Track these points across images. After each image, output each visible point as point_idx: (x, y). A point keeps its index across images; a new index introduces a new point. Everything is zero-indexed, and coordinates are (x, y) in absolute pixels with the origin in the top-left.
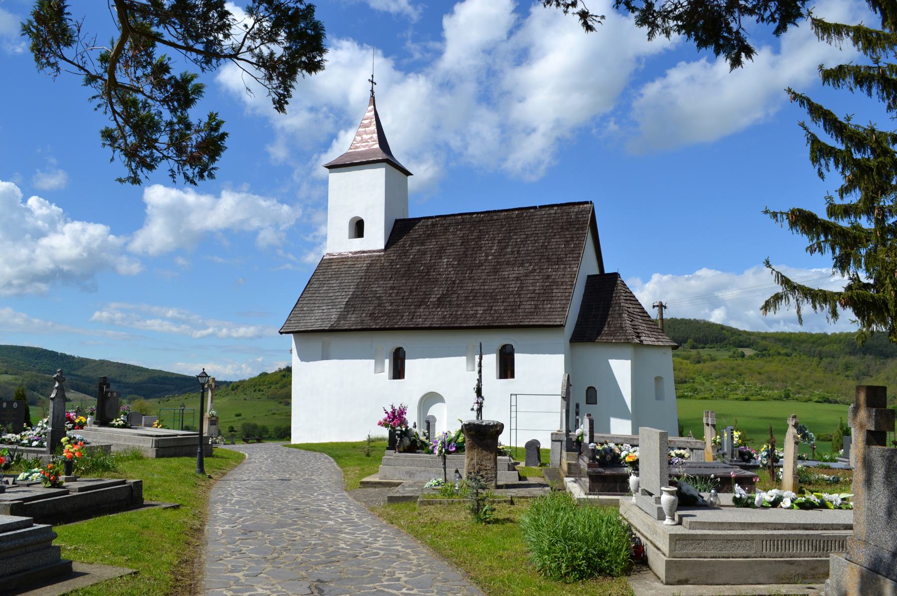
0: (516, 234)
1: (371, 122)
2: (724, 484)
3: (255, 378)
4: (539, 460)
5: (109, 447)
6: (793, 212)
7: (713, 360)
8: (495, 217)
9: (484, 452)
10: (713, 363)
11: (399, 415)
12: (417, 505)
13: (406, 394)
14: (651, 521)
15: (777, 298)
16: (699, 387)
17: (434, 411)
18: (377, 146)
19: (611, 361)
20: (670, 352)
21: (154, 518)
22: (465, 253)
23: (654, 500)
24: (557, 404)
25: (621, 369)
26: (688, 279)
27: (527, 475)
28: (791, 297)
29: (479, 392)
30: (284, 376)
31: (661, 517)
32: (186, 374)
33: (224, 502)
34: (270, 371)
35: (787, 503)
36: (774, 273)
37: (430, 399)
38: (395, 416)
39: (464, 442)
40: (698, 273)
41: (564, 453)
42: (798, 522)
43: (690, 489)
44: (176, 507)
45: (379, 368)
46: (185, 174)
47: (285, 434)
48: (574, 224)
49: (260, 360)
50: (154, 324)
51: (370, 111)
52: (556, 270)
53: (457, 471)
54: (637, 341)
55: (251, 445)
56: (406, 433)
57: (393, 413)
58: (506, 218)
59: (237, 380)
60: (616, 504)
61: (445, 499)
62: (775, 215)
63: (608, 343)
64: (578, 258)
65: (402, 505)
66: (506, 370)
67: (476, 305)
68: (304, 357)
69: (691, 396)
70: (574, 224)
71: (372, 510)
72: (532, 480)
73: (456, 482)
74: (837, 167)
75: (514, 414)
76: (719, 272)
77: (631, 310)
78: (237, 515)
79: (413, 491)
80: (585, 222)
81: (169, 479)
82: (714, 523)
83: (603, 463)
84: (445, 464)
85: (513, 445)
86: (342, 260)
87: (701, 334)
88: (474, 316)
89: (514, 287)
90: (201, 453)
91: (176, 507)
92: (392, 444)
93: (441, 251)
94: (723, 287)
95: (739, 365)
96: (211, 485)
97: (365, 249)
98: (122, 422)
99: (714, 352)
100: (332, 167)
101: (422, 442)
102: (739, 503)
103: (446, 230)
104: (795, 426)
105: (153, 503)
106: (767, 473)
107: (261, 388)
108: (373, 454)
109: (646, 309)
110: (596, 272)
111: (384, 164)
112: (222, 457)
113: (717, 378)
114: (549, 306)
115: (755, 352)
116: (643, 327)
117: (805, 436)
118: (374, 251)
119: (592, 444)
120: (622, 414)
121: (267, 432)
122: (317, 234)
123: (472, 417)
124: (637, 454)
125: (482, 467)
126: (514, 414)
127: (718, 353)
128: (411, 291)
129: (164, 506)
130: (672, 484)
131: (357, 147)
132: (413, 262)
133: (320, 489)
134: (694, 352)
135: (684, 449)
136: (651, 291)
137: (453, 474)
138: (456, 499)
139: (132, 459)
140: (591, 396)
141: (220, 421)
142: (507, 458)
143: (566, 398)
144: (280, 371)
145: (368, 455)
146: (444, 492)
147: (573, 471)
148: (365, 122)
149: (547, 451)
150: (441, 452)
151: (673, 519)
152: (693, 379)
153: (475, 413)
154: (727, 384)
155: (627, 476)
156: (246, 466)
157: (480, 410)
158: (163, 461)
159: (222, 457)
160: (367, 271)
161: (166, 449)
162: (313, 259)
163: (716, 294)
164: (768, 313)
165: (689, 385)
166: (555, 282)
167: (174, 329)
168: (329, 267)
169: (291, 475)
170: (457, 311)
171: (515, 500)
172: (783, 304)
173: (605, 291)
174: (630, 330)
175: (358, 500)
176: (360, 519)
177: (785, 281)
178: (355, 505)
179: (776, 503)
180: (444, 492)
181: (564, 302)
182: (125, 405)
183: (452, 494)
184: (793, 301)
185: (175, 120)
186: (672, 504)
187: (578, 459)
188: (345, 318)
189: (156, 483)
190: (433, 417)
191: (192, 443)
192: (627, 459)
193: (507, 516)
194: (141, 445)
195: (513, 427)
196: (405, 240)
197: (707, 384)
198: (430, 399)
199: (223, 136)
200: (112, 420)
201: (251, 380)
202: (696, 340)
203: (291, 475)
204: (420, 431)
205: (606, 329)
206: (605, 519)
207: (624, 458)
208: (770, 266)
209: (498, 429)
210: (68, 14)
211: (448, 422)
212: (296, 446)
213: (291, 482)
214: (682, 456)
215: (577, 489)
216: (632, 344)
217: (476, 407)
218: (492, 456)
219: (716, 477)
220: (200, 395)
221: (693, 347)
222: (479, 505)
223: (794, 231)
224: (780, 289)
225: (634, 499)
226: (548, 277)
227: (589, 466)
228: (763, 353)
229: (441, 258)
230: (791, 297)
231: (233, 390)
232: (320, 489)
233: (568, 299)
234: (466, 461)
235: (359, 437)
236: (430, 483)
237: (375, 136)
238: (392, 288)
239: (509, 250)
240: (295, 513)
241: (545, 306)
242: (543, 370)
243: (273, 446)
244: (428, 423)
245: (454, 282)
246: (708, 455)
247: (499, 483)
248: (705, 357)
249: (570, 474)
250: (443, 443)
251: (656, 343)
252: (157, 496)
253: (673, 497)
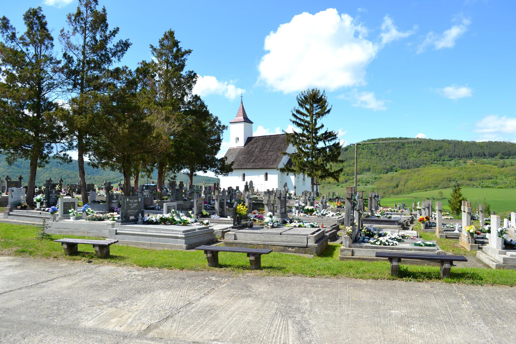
7: (512, 165)
10: (513, 167)
69: (492, 187)
74: (181, 184)
87: (507, 150)
165: (493, 180)
196: (249, 144)
197: (505, 180)
202: (503, 154)
221: (502, 158)
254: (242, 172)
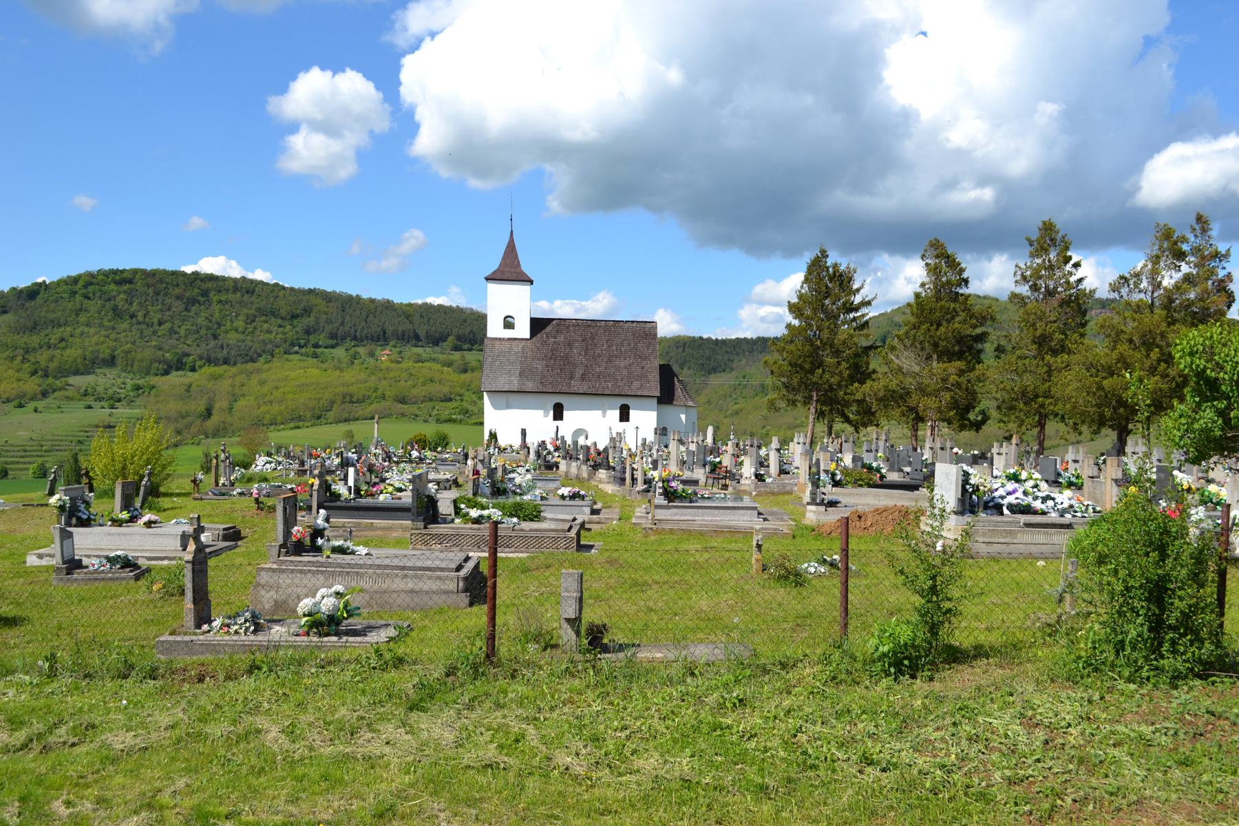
16: (470, 408)
45: (546, 415)
69: (461, 421)
87: (468, 330)
134: (457, 356)
195: (22, 453)
202: (459, 338)
221: (456, 348)
242: (645, 421)
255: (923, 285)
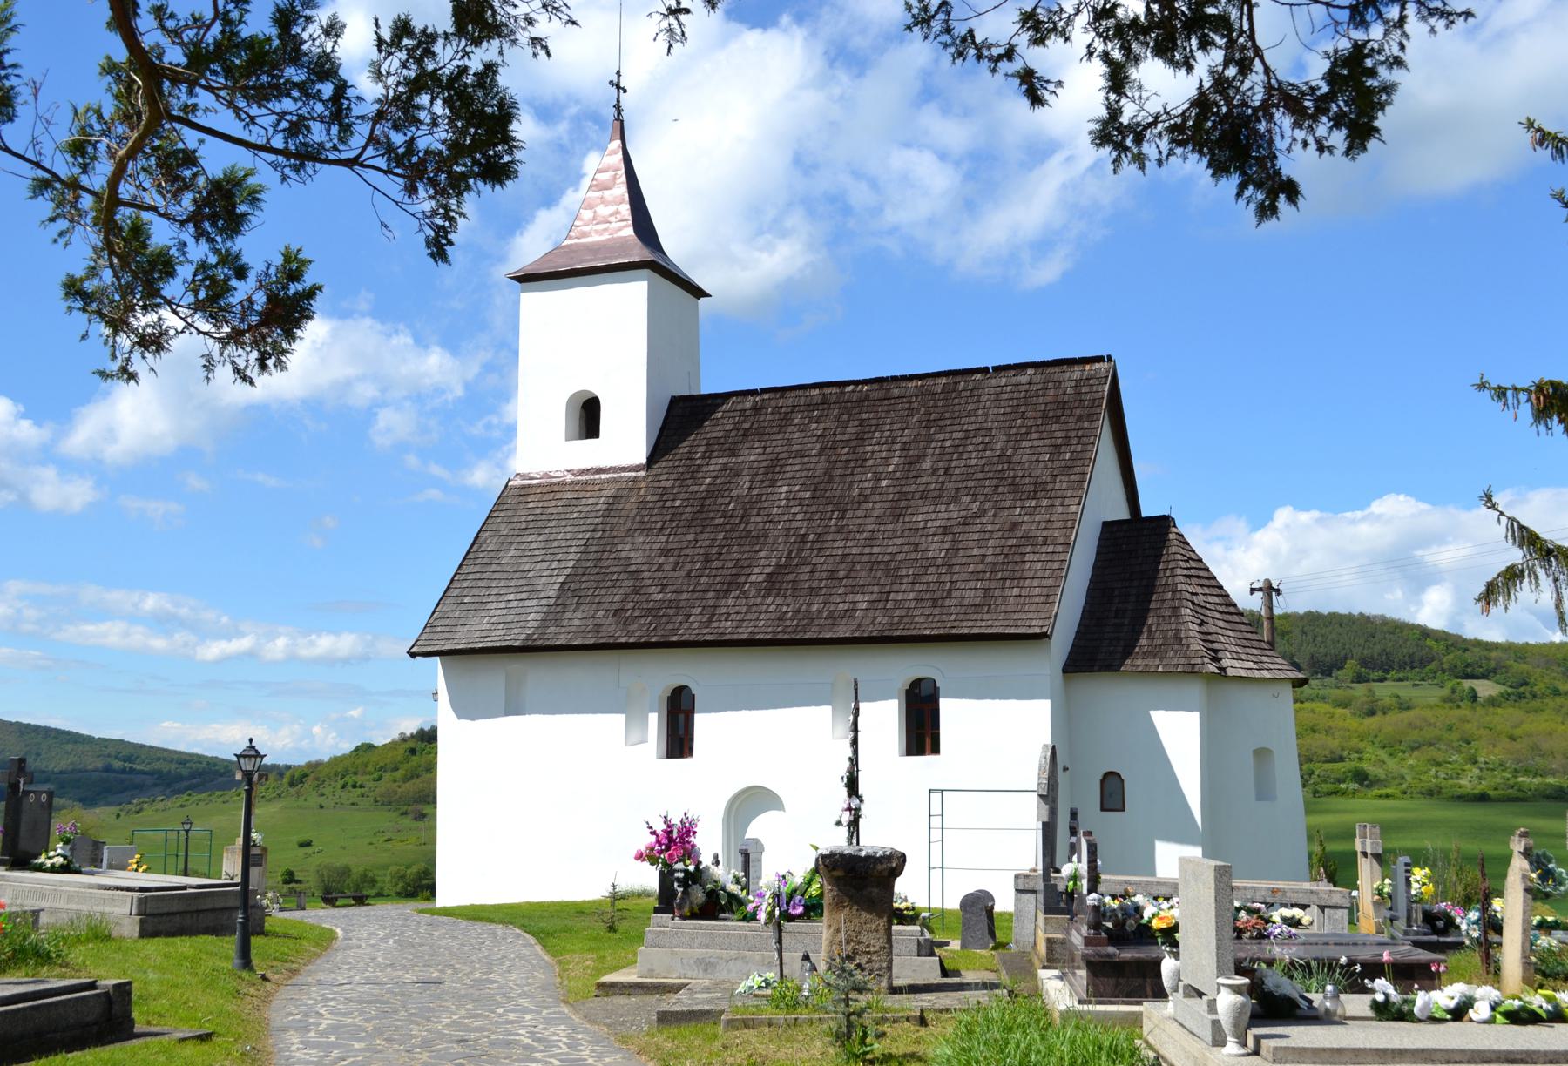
0: (941, 429)
1: (615, 178)
2: (1355, 977)
3: (344, 757)
4: (992, 934)
5: (36, 914)
6: (1540, 388)
7: (1404, 706)
8: (896, 392)
9: (865, 916)
11: (681, 838)
12: (720, 1029)
13: (695, 792)
14: (1198, 1047)
15: (1512, 576)
17: (758, 828)
18: (630, 231)
19: (1152, 713)
20: (1287, 692)
21: (162, 1058)
22: (828, 473)
23: (1205, 1007)
24: (1028, 813)
25: (1179, 732)
26: (1353, 522)
27: (961, 967)
28: (1541, 573)
29: (852, 785)
30: (413, 751)
31: (1219, 1041)
32: (179, 748)
33: (304, 1028)
34: (380, 740)
35: (1481, 1011)
36: (1504, 520)
37: (752, 801)
38: (671, 840)
39: (821, 896)
40: (1377, 507)
41: (1041, 917)
42: (1496, 1047)
43: (1276, 981)
44: (204, 1038)
45: (634, 733)
46: (233, 363)
47: (421, 885)
48: (1075, 404)
49: (355, 713)
50: (111, 633)
51: (614, 152)
52: (1033, 511)
53: (806, 957)
54: (1212, 668)
55: (344, 911)
56: (696, 877)
57: (668, 832)
58: (921, 393)
59: (301, 761)
60: (1136, 1020)
61: (780, 1016)
62: (1501, 393)
63: (1146, 673)
64: (1080, 484)
65: (687, 1030)
66: (922, 734)
67: (854, 589)
68: (465, 710)
69: (1354, 792)
70: (1075, 404)
71: (624, 1040)
72: (969, 977)
73: (803, 980)
75: (936, 835)
76: (1424, 506)
77: (1199, 599)
78: (335, 1053)
79: (711, 1001)
80: (1095, 403)
81: (180, 981)
82: (1324, 1050)
83: (1119, 937)
84: (780, 941)
85: (936, 904)
86: (551, 489)
87: (1378, 648)
88: (849, 614)
89: (937, 548)
90: (244, 925)
91: (204, 1038)
92: (666, 901)
93: (774, 469)
94: (1437, 538)
95: (1464, 720)
96: (269, 994)
97: (603, 465)
98: (60, 860)
99: (1406, 691)
100: (528, 279)
101: (732, 896)
102: (1384, 1011)
103: (786, 420)
104: (1526, 853)
105: (153, 1029)
106: (1476, 958)
107: (360, 779)
108: (622, 926)
109: (1234, 597)
110: (1123, 514)
111: (646, 272)
112: (286, 936)
113: (1413, 749)
114: (1016, 591)
115: (1502, 689)
116: (1225, 638)
117: (1546, 875)
118: (624, 469)
119: (1094, 895)
120: (1181, 832)
121: (373, 882)
122: (495, 420)
123: (837, 840)
124: (1175, 912)
125: (861, 948)
126: (936, 835)
127: (1415, 692)
128: (707, 559)
129: (181, 1035)
130: (1240, 970)
131: (584, 235)
132: (710, 493)
133: (510, 1000)
134: (1360, 690)
135: (1304, 907)
136: (1245, 555)
137: (798, 963)
138: (803, 1014)
139: (88, 940)
140: (1112, 792)
141: (270, 857)
142: (917, 928)
143: (1049, 796)
144: (404, 739)
145: (612, 929)
146: (778, 1001)
147: (1056, 956)
148: (602, 177)
149: (1009, 917)
150: (771, 915)
151: (1245, 1045)
152: (1359, 752)
153: (844, 832)
154: (1438, 764)
155: (1157, 964)
156: (340, 956)
157: (854, 824)
158: (155, 946)
159: (286, 936)
160: (607, 514)
161: (163, 917)
162: (486, 481)
163: (1419, 553)
164: (1493, 609)
166: (1028, 538)
167: (159, 643)
168: (521, 505)
169: (442, 971)
170: (810, 604)
171: (930, 1016)
172: (1524, 592)
173: (1140, 556)
174: (1197, 645)
175: (593, 1022)
176: (599, 1058)
177: (1527, 538)
178: (586, 1031)
179: (1459, 1013)
180: (778, 1001)
181: (1050, 582)
182: (64, 821)
183: (796, 1004)
184: (1546, 582)
185: (213, 259)
186: (1238, 1012)
187: (1067, 931)
188: (557, 622)
189: (154, 989)
190: (757, 842)
191: (219, 904)
192: (1156, 924)
193: (910, 1050)
194: (107, 909)
195: (936, 862)
196: (693, 444)
197: (1392, 764)
198: (752, 801)
199: (311, 293)
200: (37, 856)
201: (335, 761)
202: (1364, 663)
203: (442, 971)
204: (725, 875)
205: (1143, 641)
206: (1106, 1044)
207: (1150, 921)
208: (1493, 507)
209: (892, 865)
210: (14, 66)
211: (790, 851)
212: (447, 912)
213: (445, 987)
214: (1295, 923)
215: (1060, 992)
216: (1204, 676)
217: (846, 817)
218: (882, 922)
219: (1351, 963)
220: (244, 795)
221: (1360, 679)
222: (850, 1025)
223: (1542, 428)
224: (1516, 556)
225: (1169, 1008)
226: (1014, 526)
227: (1088, 942)
228: (1521, 692)
229: (773, 484)
230: (1541, 573)
231: (292, 784)
232: (510, 1000)
233: (1059, 575)
234: (826, 935)
235: (590, 888)
236: (749, 983)
237: (625, 209)
238: (665, 552)
239: (926, 466)
240: (458, 1049)
241: (1007, 592)
242: (1003, 734)
243: (394, 914)
244: (746, 856)
245: (804, 537)
246: (1369, 920)
247: (896, 983)
248: (1387, 701)
249: (1050, 962)
250: (776, 896)
251: (1257, 674)
252: (160, 1015)
253: (1239, 999)
254: (660, 674)
255: (945, 46)
